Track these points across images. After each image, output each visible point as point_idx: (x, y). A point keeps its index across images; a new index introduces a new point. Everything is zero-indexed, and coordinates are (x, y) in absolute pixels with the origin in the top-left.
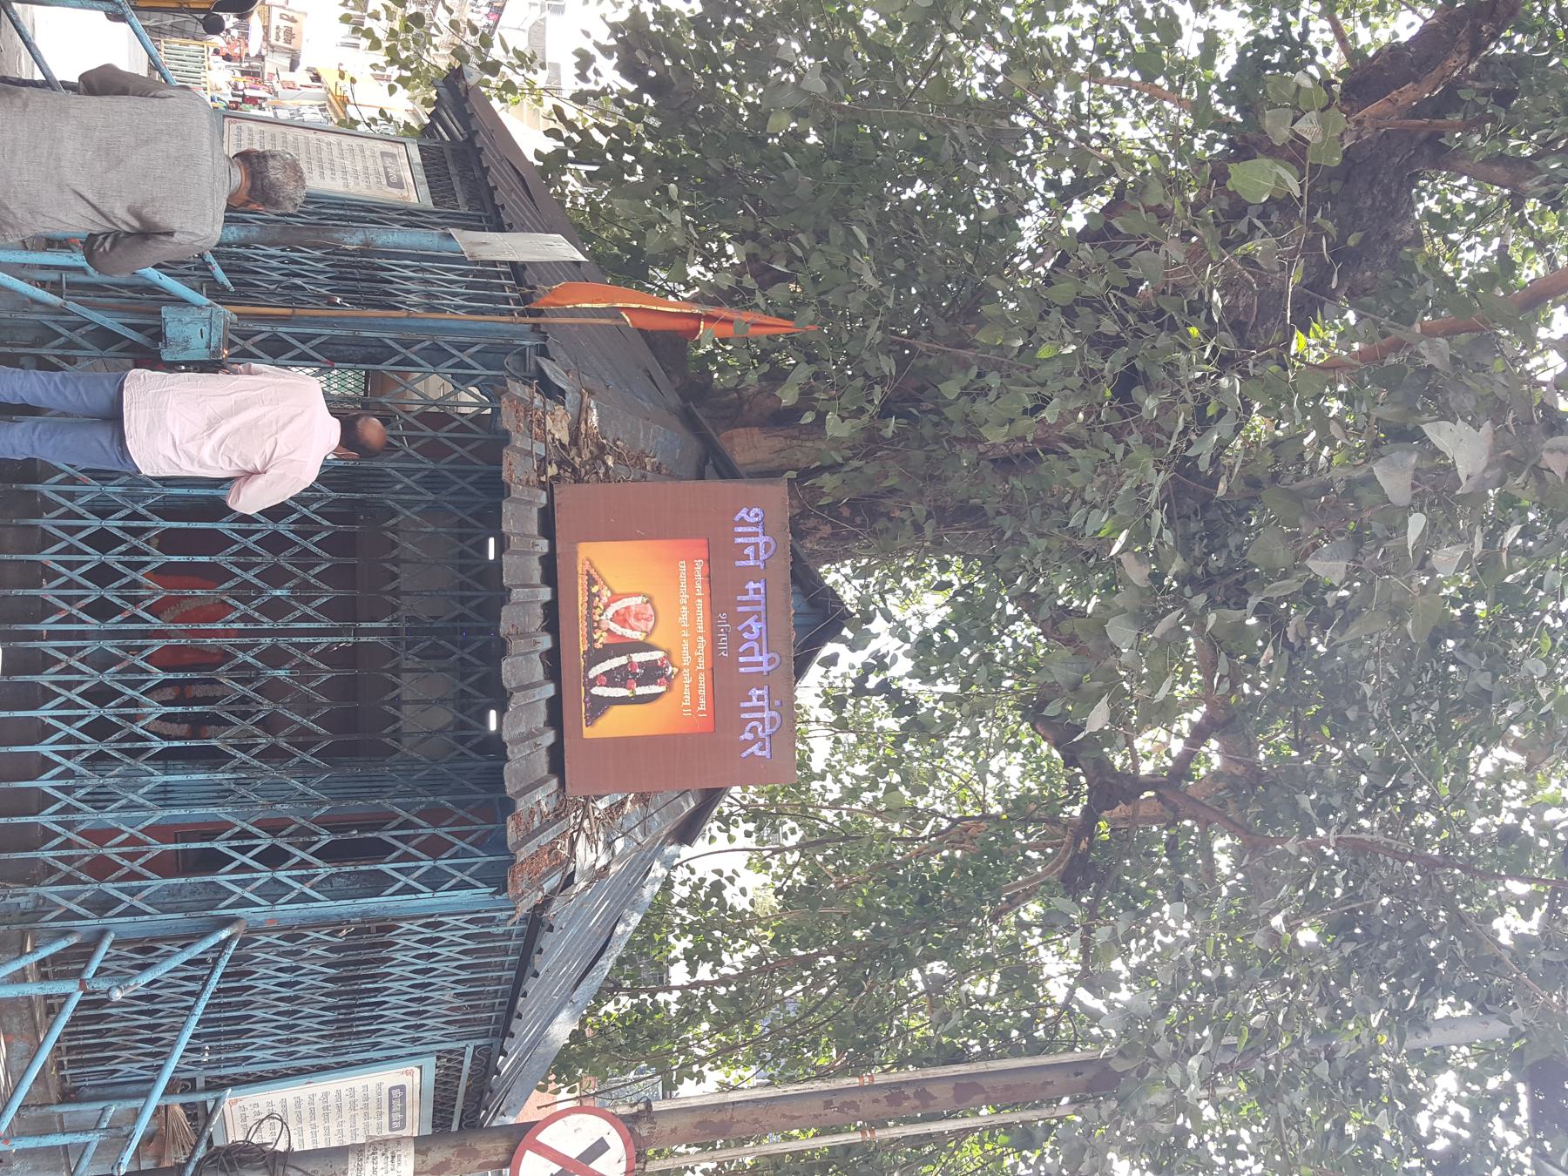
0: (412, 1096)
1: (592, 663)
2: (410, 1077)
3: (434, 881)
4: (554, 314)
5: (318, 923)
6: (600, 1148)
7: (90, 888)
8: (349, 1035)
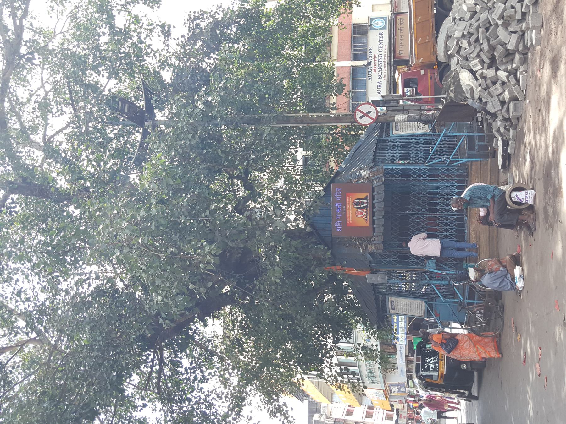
0: (394, 128)
1: (367, 206)
2: (395, 133)
3: (392, 170)
4: (367, 270)
5: (412, 164)
6: (361, 118)
7: (450, 173)
8: (406, 141)
